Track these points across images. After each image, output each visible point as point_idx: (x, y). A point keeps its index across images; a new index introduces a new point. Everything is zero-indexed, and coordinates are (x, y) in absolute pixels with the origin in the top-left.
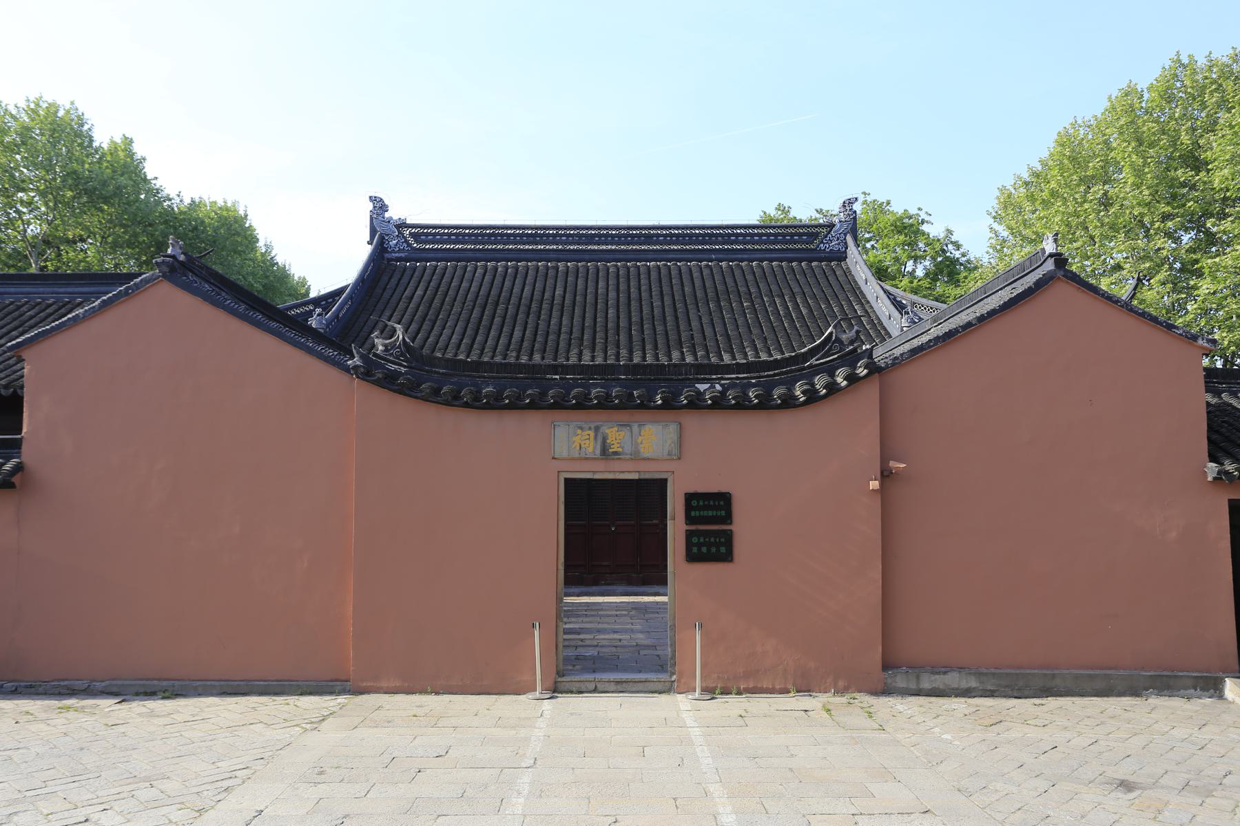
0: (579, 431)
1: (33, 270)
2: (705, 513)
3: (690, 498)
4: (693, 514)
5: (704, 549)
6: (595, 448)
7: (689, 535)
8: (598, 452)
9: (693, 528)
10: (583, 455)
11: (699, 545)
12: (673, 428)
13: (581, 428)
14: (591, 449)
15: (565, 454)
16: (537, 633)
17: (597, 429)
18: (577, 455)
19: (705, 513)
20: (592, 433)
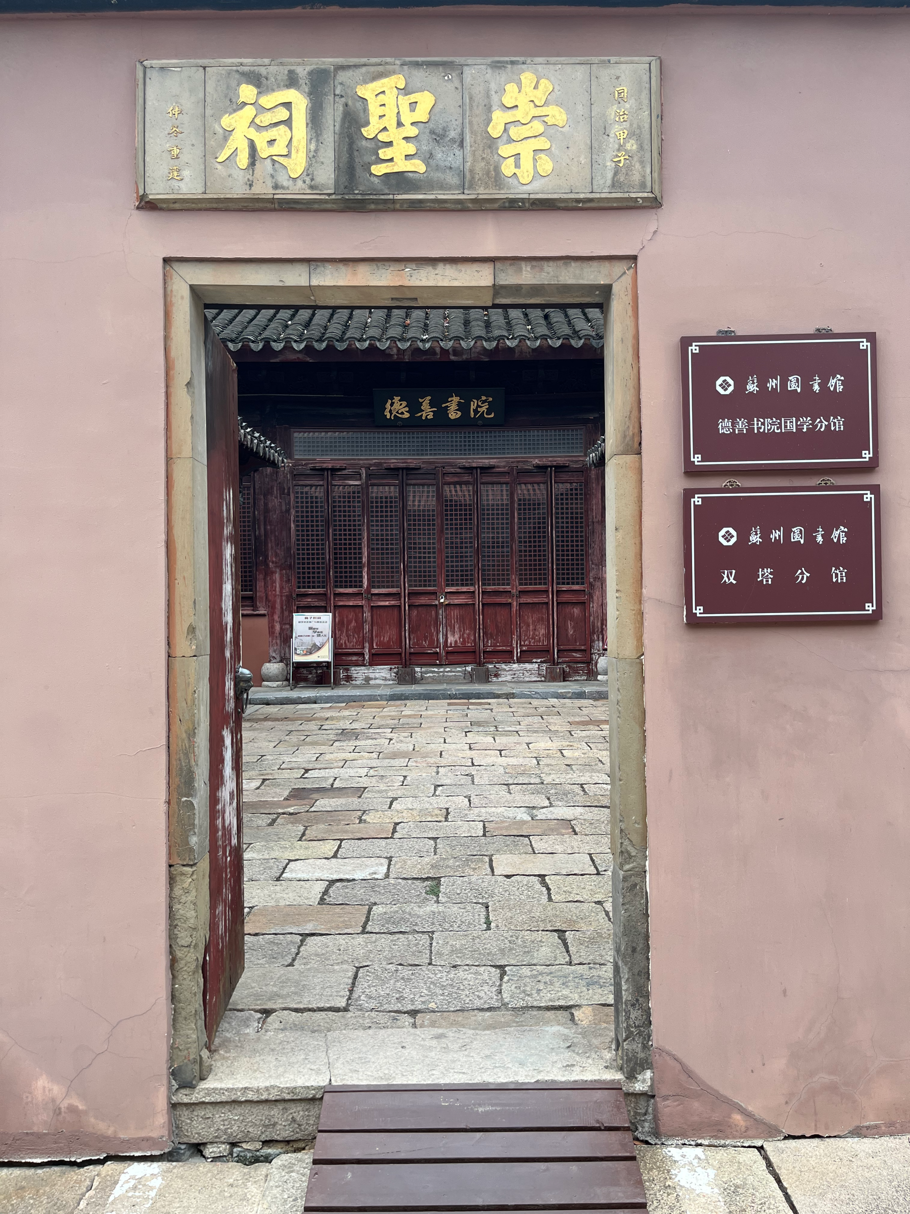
0: (247, 92)
1: (392, 488)
2: (765, 425)
3: (707, 361)
4: (724, 426)
5: (765, 575)
6: (313, 158)
7: (700, 523)
8: (326, 176)
9: (840, 487)
10: (263, 189)
11: (741, 557)
12: (580, 72)
13: (257, 81)
14: (297, 165)
15: (189, 186)
16: (400, 197)
17: (318, 86)
18: (238, 190)
19: (765, 425)
20: (300, 101)
